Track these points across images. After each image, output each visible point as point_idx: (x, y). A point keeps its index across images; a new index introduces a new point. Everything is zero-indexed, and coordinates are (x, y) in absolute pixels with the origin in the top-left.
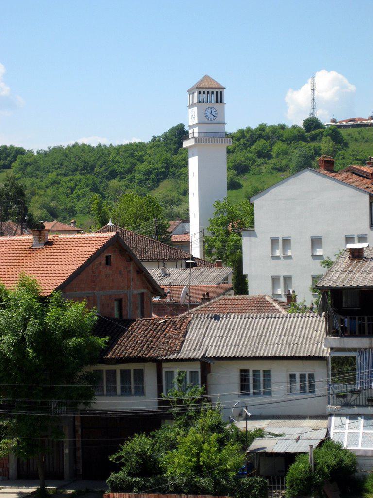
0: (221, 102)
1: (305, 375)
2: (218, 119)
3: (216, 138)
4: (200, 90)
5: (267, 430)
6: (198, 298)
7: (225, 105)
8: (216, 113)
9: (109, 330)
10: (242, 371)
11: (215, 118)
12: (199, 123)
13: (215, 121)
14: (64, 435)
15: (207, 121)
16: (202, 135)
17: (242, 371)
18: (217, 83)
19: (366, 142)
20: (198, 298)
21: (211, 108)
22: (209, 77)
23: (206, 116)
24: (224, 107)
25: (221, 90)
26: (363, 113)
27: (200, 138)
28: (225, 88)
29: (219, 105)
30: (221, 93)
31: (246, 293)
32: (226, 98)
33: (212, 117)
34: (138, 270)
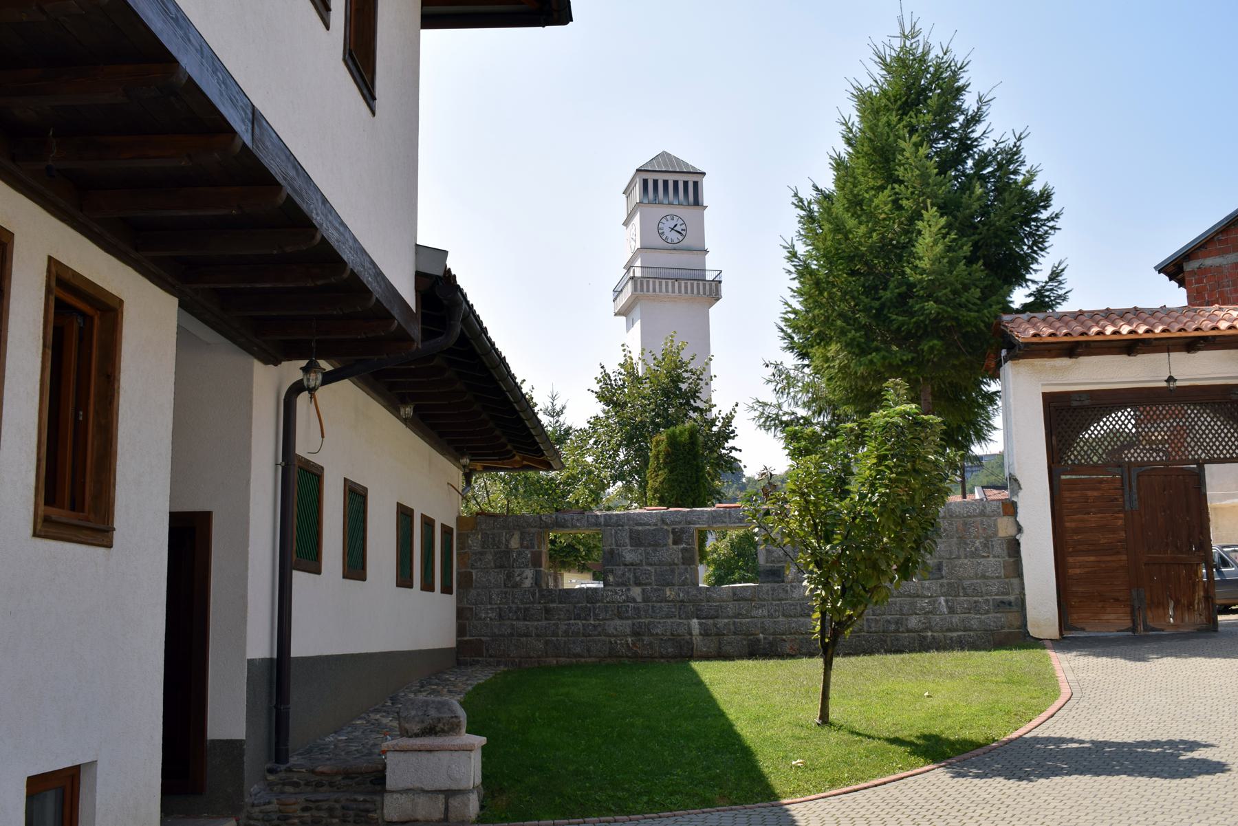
1: (443, 592)
2: (687, 242)
4: (646, 176)
5: (260, 646)
6: (602, 370)
7: (706, 212)
8: (684, 227)
10: (644, 180)
12: (643, 248)
15: (660, 243)
16: (650, 273)
17: (644, 180)
18: (693, 167)
20: (602, 370)
21: (672, 217)
22: (669, 155)
23: (661, 235)
25: (695, 178)
27: (645, 280)
28: (704, 174)
29: (693, 211)
30: (696, 184)
32: (707, 196)
33: (674, 236)
34: (1226, 768)
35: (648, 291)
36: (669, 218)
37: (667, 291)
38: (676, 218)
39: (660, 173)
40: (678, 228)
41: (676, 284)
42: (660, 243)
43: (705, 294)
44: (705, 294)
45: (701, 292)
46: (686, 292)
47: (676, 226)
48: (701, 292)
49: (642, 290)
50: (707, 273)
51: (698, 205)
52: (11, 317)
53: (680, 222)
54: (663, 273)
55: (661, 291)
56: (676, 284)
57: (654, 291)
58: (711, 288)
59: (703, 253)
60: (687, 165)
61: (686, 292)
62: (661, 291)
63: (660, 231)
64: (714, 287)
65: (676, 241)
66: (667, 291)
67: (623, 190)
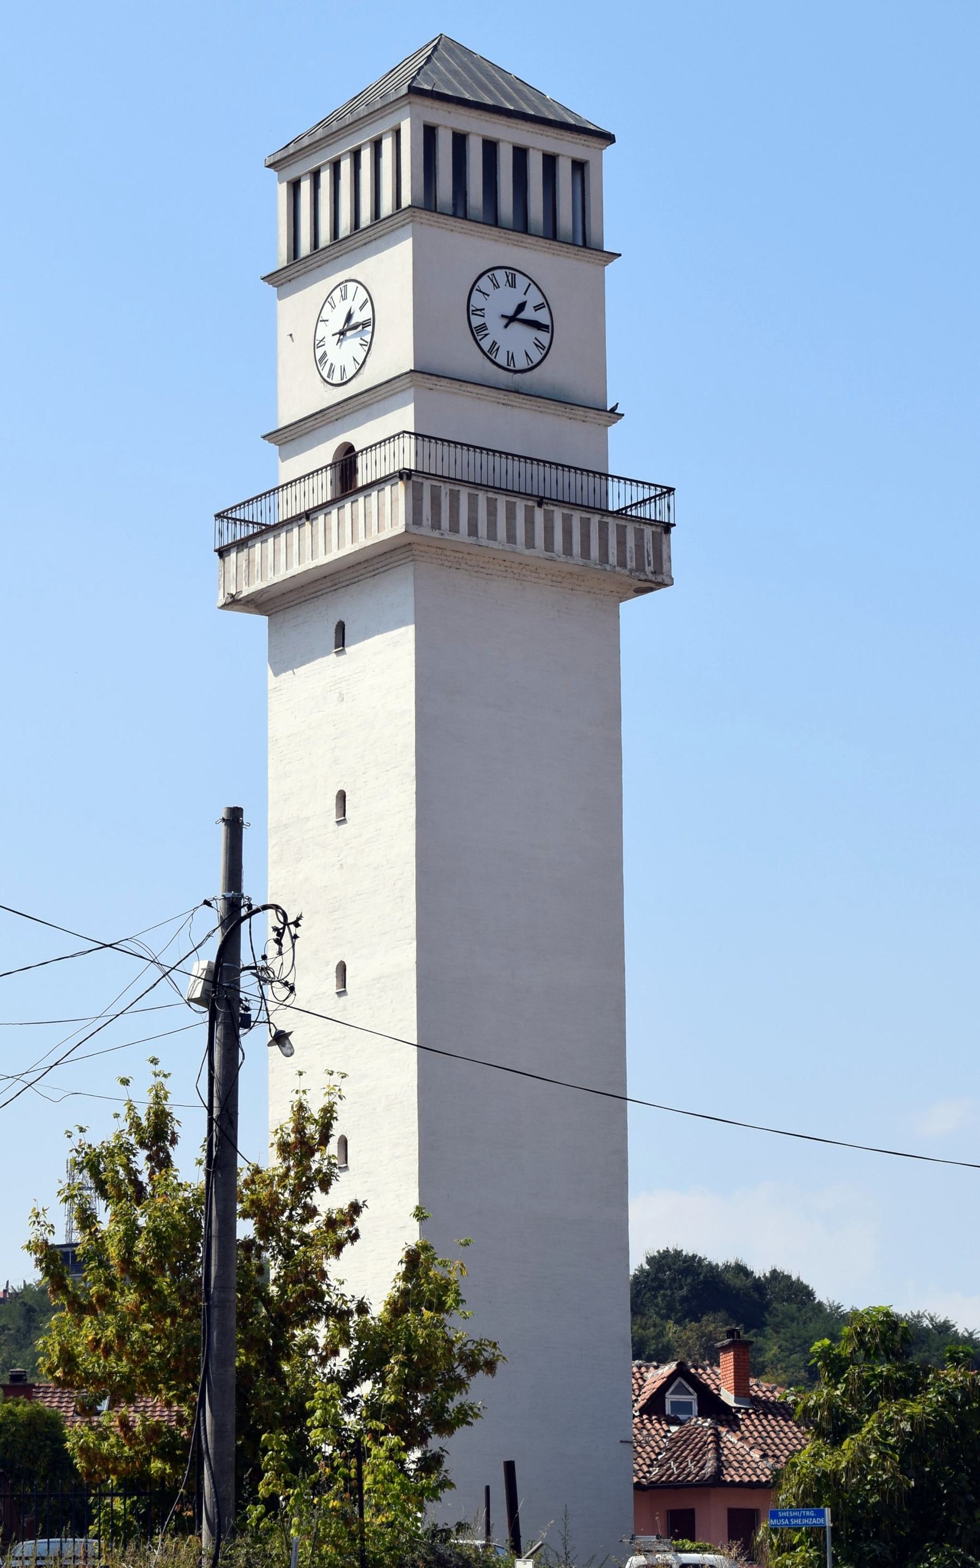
3: (558, 514)
15: (475, 364)
21: (513, 274)
23: (477, 332)
28: (609, 138)
30: (579, 167)
35: (454, 528)
36: (500, 275)
37: (511, 538)
38: (521, 281)
39: (475, 114)
40: (528, 314)
41: (539, 514)
42: (475, 364)
43: (622, 563)
44: (622, 563)
45: (613, 558)
46: (568, 550)
47: (521, 307)
48: (613, 558)
49: (436, 525)
50: (613, 486)
51: (585, 245)
52: (505, 1501)
53: (534, 298)
54: (513, 473)
55: (492, 535)
56: (539, 514)
57: (473, 531)
58: (639, 546)
59: (604, 417)
60: (519, 85)
61: (568, 550)
62: (492, 535)
63: (476, 321)
64: (649, 545)
65: (521, 363)
66: (511, 538)
67: (275, 144)
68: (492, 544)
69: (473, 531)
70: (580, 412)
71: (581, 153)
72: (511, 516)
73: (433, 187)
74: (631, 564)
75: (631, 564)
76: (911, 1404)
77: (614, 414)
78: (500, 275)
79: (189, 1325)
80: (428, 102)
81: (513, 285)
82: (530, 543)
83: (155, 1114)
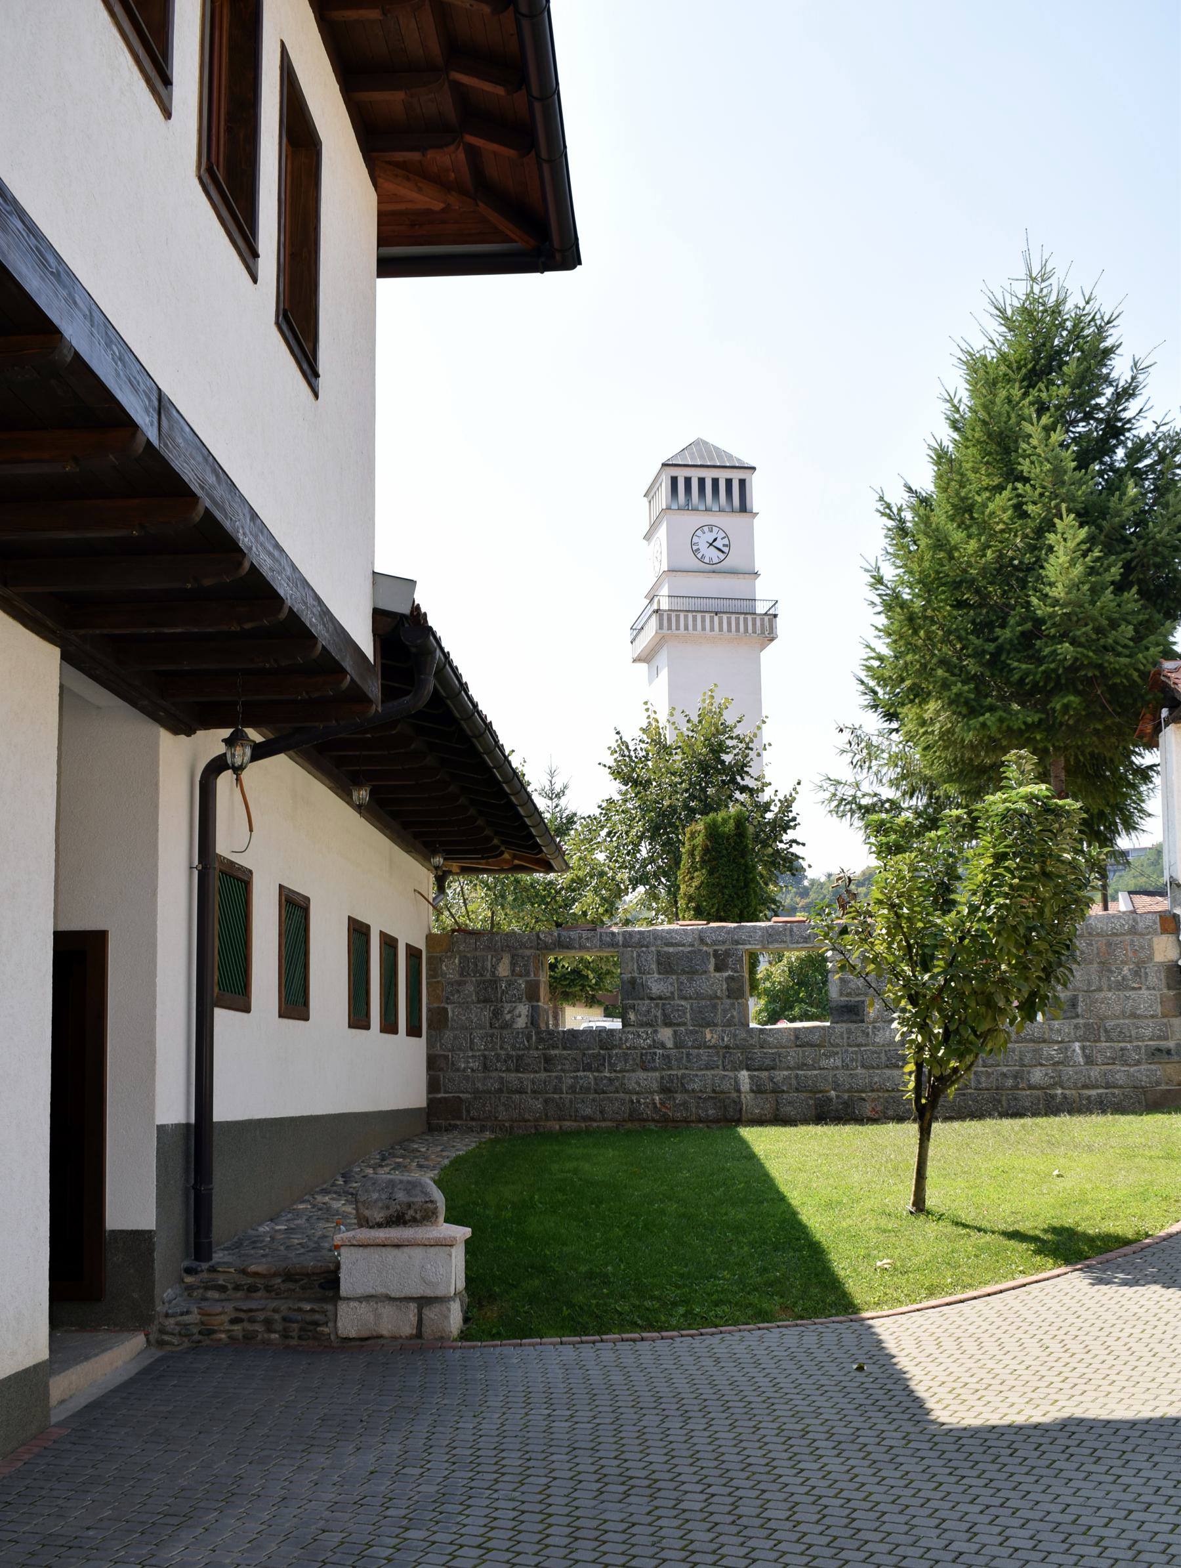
0: (744, 508)
3: (725, 617)
6: (618, 737)
7: (756, 521)
8: (726, 541)
9: (939, 974)
11: (722, 556)
13: (729, 563)
14: (894, 1357)
15: (694, 563)
18: (730, 457)
19: (939, 1219)
20: (618, 737)
21: (711, 527)
23: (695, 552)
24: (751, 528)
25: (736, 476)
26: (1172, 1412)
28: (754, 469)
29: (740, 519)
30: (742, 482)
31: (388, 267)
36: (706, 529)
39: (693, 469)
40: (718, 544)
41: (716, 619)
42: (694, 563)
43: (754, 632)
44: (754, 632)
47: (715, 540)
49: (670, 628)
54: (704, 604)
56: (716, 619)
57: (686, 628)
58: (762, 625)
59: (753, 576)
63: (695, 548)
65: (715, 560)
66: (704, 629)
68: (695, 632)
69: (686, 628)
70: (741, 576)
71: (742, 477)
72: (703, 621)
73: (284, 954)
74: (758, 632)
75: (758, 632)
76: (1141, 617)
77: (756, 574)
78: (706, 529)
79: (910, 521)
80: (672, 468)
81: (711, 531)
82: (712, 629)
83: (537, 848)
